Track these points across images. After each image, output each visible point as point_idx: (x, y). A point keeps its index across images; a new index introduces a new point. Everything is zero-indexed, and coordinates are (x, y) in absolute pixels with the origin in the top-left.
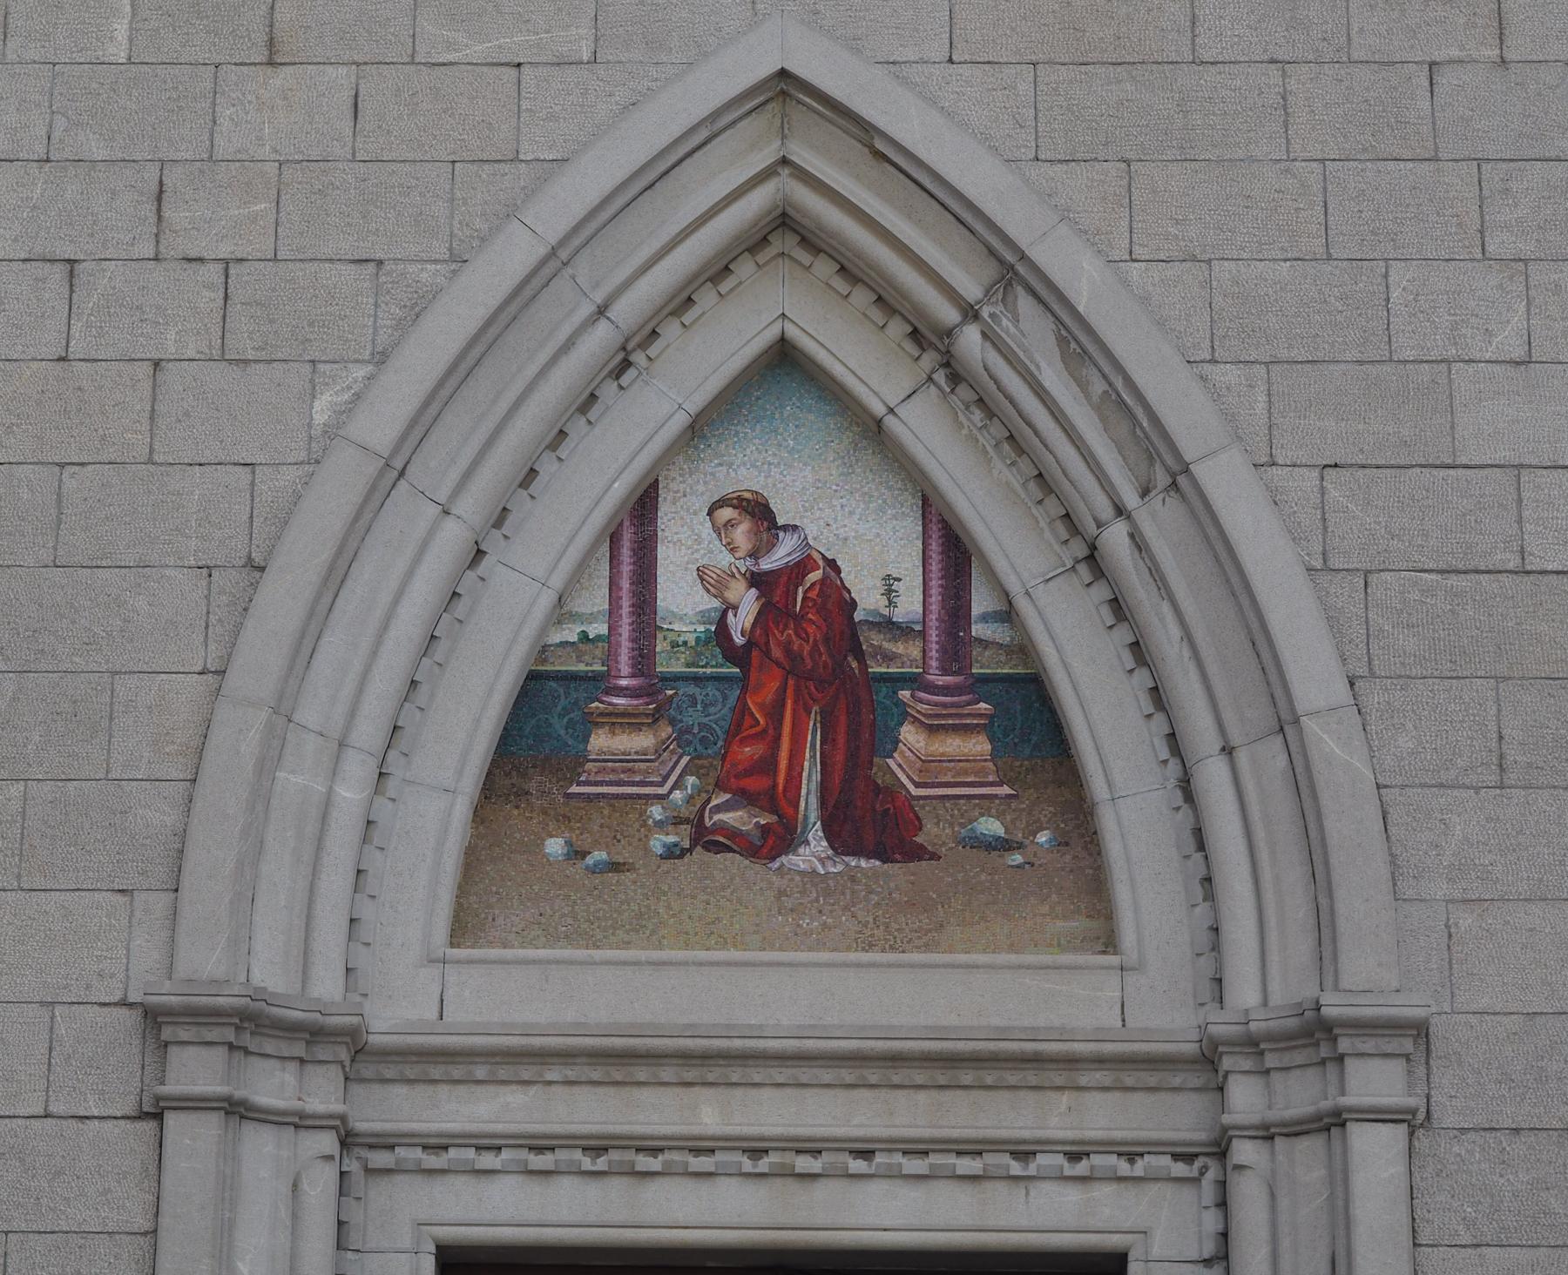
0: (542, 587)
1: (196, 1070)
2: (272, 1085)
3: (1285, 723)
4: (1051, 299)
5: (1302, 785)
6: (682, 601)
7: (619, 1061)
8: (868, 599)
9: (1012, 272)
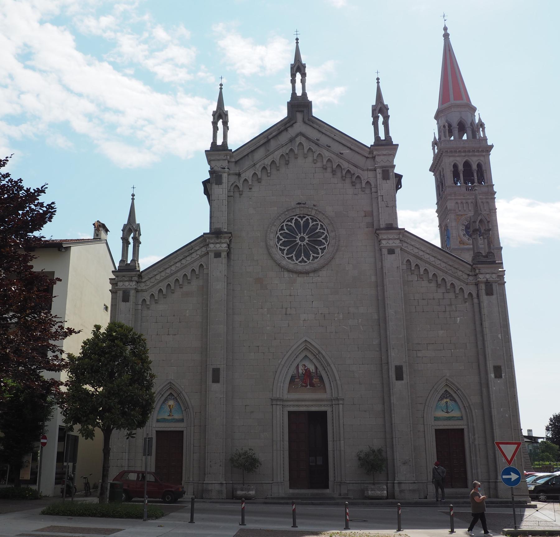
0: (292, 371)
1: (274, 403)
2: (279, 403)
3: (336, 380)
4: (322, 354)
5: (337, 384)
6: (300, 371)
7: (298, 400)
8: (311, 371)
9: (319, 352)
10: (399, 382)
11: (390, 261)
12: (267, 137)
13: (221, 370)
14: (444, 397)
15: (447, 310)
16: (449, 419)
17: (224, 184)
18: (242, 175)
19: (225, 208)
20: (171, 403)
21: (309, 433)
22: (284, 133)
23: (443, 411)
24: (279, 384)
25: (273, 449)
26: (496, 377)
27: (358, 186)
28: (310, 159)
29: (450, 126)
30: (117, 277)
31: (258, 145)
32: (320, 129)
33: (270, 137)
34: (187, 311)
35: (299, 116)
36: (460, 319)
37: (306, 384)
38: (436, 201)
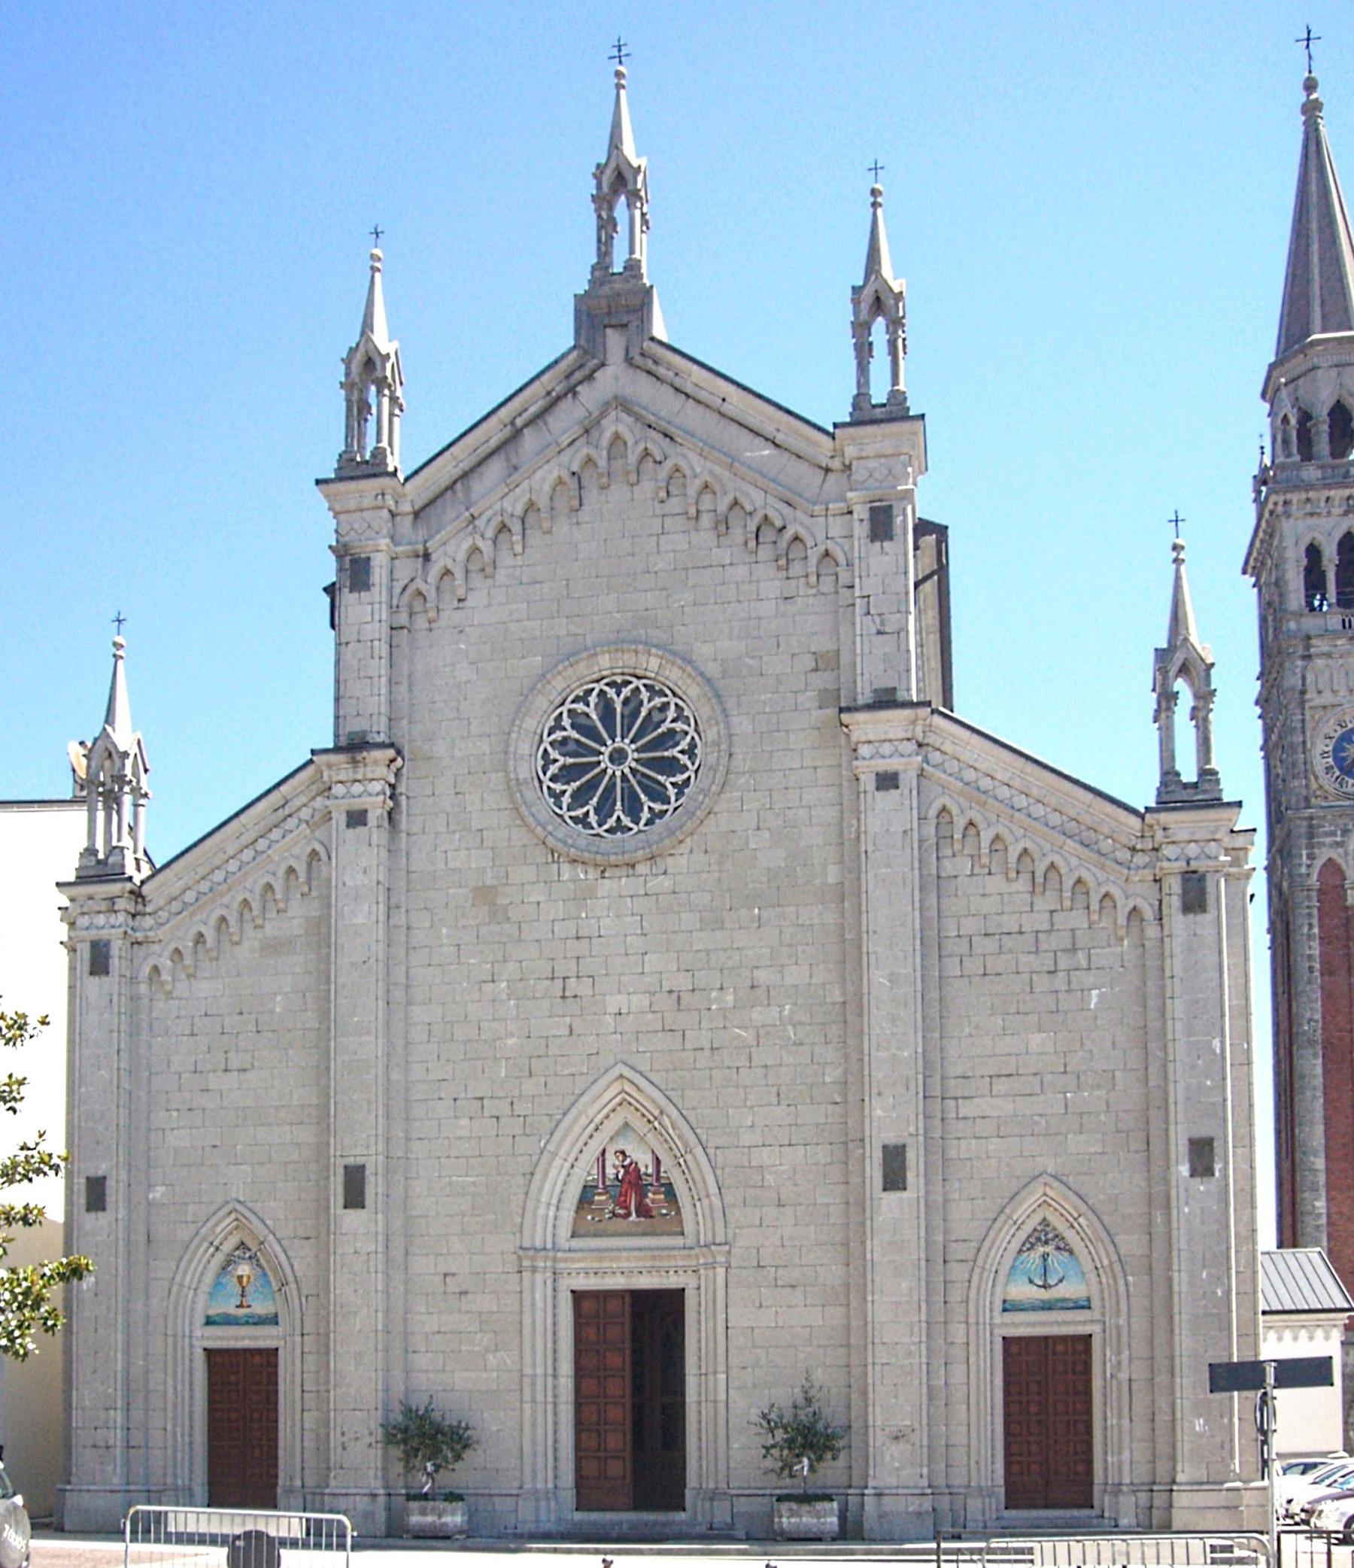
0: (585, 1171)
6: (610, 1172)
10: (893, 1196)
11: (888, 816)
12: (513, 423)
13: (369, 1172)
14: (1039, 1239)
15: (1062, 965)
16: (1048, 1306)
17: (375, 590)
18: (434, 557)
19: (379, 667)
20: (244, 1269)
21: (635, 1349)
22: (566, 404)
23: (1031, 1282)
24: (541, 1211)
25: (526, 1403)
26: (1193, 1174)
27: (796, 569)
28: (647, 487)
30: (72, 900)
31: (484, 450)
32: (678, 382)
33: (519, 422)
34: (279, 998)
35: (615, 342)
36: (1100, 996)
37: (627, 1208)
38: (1257, 669)
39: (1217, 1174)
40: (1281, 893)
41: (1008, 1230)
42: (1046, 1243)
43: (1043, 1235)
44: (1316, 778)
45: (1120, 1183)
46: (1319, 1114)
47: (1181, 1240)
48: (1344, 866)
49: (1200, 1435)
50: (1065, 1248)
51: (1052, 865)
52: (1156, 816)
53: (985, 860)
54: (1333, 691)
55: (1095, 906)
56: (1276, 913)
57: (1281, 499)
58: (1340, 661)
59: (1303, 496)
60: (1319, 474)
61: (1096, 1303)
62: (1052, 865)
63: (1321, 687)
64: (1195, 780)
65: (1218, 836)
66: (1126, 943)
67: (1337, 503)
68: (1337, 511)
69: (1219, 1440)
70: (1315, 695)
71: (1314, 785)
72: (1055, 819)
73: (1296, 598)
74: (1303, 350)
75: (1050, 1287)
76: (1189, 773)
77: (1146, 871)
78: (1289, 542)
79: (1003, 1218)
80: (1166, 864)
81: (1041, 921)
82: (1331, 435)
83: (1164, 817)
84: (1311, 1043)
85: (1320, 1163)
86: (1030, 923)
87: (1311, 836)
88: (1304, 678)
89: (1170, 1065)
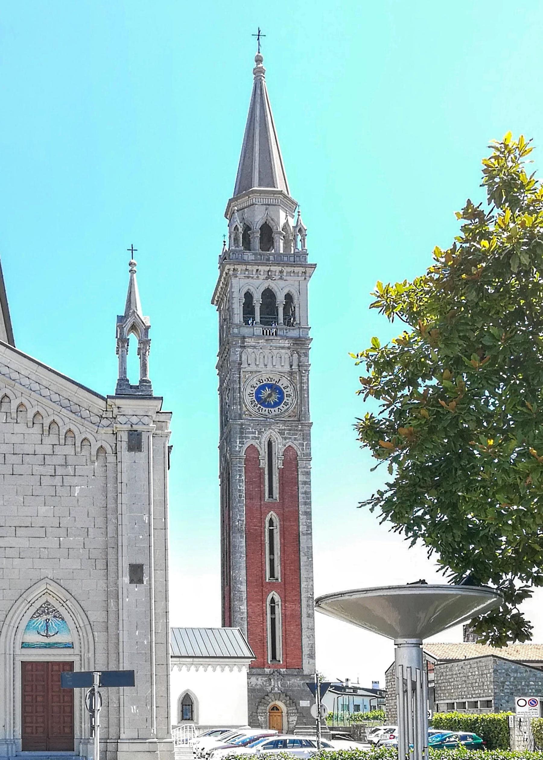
26: (131, 581)
29: (247, 228)
36: (81, 490)
39: (145, 583)
40: (226, 460)
41: (24, 606)
42: (48, 613)
43: (45, 609)
44: (246, 406)
45: (91, 585)
46: (243, 565)
47: (124, 615)
48: (259, 449)
49: (135, 715)
50: (58, 616)
51: (54, 422)
52: (113, 400)
53: (14, 415)
54: (256, 365)
55: (78, 444)
56: (224, 469)
57: (232, 268)
58: (261, 351)
59: (244, 267)
60: (253, 257)
61: (76, 645)
62: (54, 422)
63: (249, 362)
64: (138, 385)
65: (149, 414)
66: (96, 464)
67: (262, 273)
68: (262, 277)
69: (145, 717)
70: (247, 366)
71: (244, 409)
72: (55, 398)
73: (238, 316)
74: (247, 195)
75: (50, 636)
76: (134, 379)
77: (109, 429)
78: (235, 290)
79: (21, 599)
80: (119, 426)
81: (48, 450)
82: (261, 239)
83: (118, 402)
84: (240, 531)
85: (243, 588)
86: (40, 449)
87: (242, 433)
88: (241, 357)
89: (120, 528)
